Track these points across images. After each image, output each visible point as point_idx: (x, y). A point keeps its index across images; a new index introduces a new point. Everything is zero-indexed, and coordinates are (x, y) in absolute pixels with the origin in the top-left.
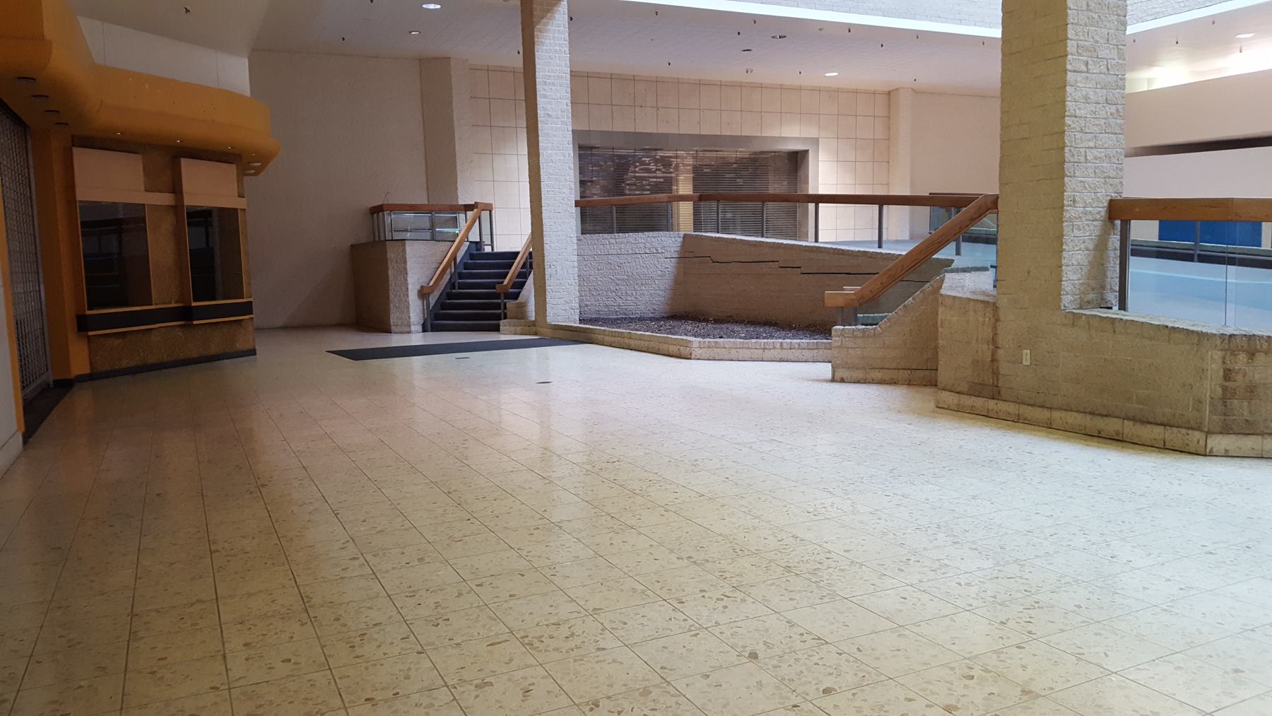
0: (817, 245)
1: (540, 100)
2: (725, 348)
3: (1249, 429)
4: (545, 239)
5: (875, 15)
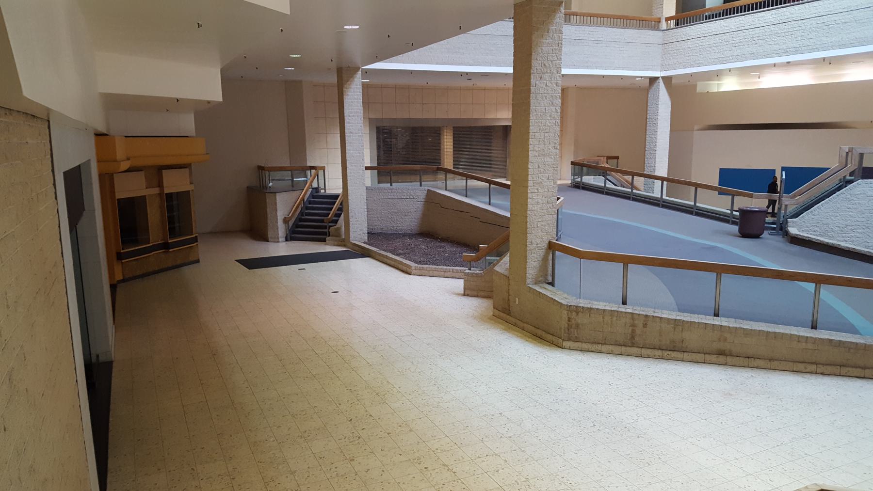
1: (346, 125)
3: (577, 340)
4: (349, 197)
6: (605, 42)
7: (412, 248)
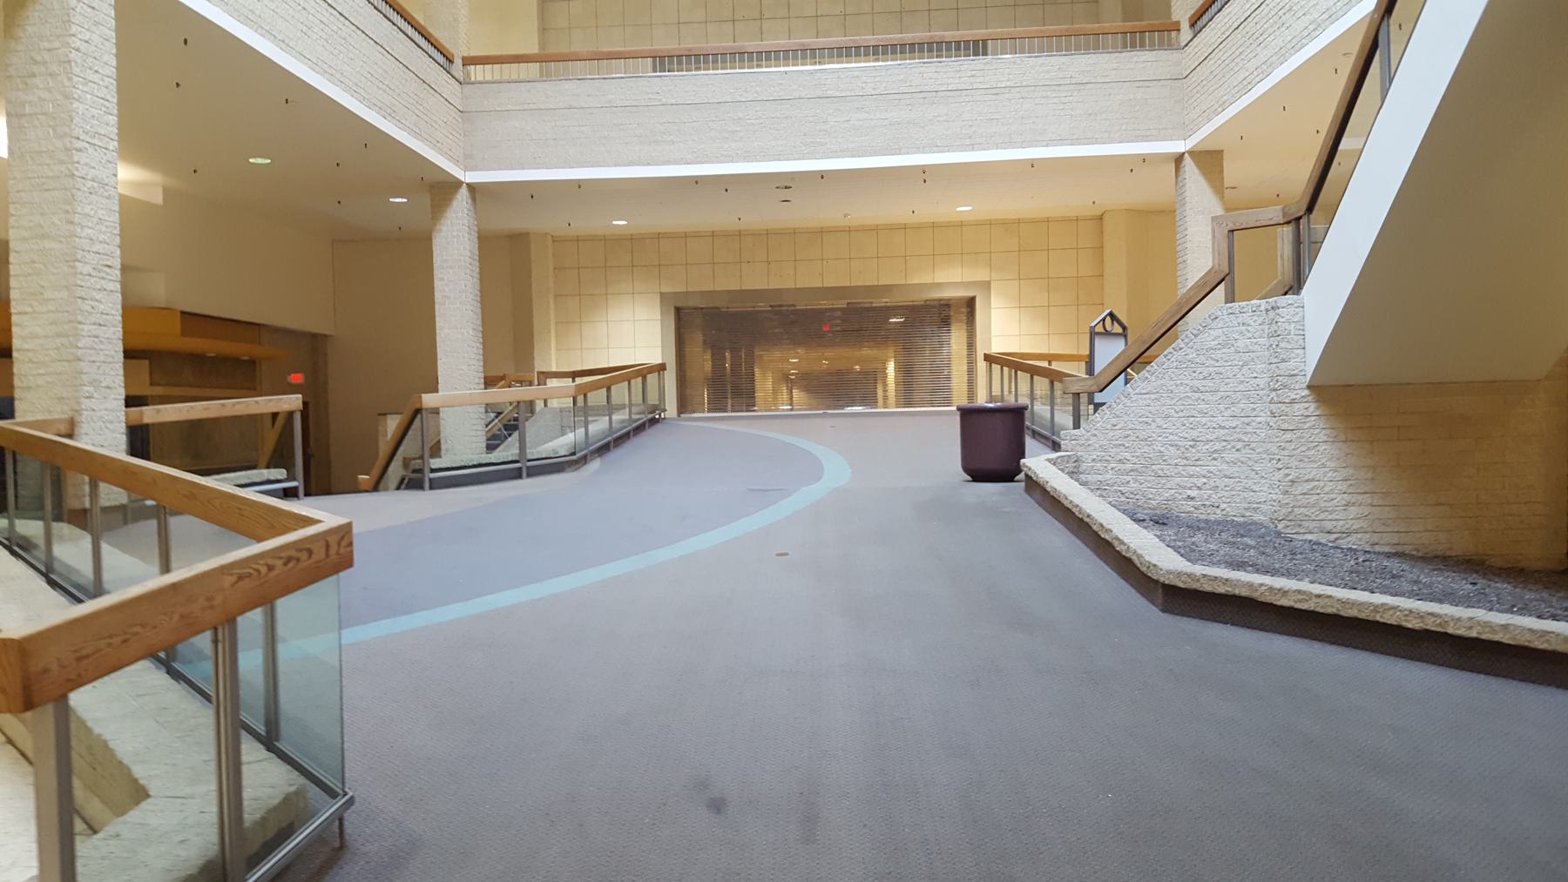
5: (838, 157)
6: (1018, 89)
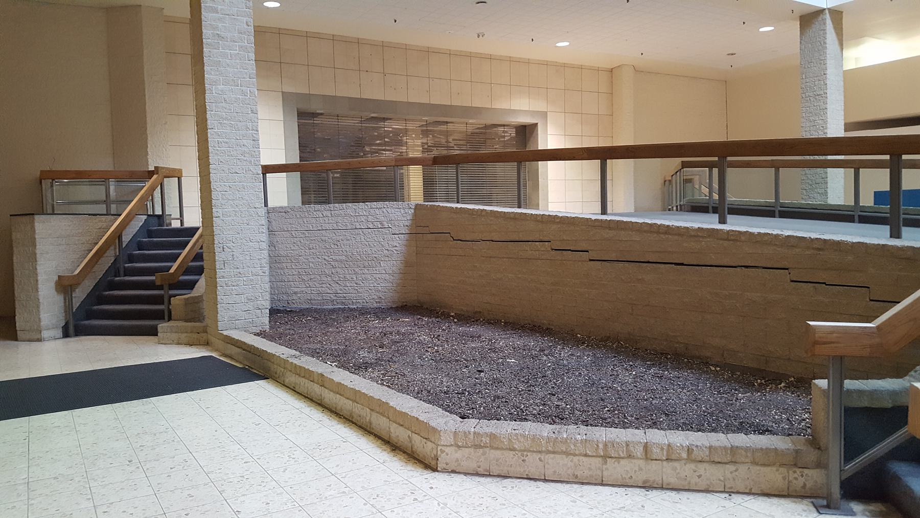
0: (604, 217)
2: (514, 450)
7: (395, 342)
